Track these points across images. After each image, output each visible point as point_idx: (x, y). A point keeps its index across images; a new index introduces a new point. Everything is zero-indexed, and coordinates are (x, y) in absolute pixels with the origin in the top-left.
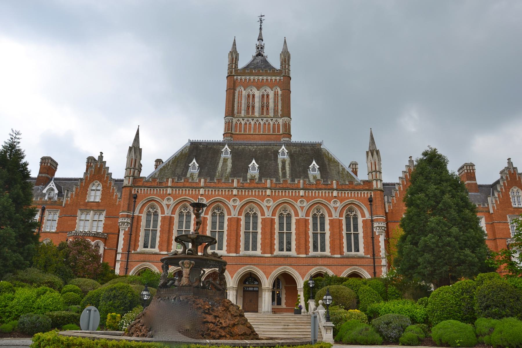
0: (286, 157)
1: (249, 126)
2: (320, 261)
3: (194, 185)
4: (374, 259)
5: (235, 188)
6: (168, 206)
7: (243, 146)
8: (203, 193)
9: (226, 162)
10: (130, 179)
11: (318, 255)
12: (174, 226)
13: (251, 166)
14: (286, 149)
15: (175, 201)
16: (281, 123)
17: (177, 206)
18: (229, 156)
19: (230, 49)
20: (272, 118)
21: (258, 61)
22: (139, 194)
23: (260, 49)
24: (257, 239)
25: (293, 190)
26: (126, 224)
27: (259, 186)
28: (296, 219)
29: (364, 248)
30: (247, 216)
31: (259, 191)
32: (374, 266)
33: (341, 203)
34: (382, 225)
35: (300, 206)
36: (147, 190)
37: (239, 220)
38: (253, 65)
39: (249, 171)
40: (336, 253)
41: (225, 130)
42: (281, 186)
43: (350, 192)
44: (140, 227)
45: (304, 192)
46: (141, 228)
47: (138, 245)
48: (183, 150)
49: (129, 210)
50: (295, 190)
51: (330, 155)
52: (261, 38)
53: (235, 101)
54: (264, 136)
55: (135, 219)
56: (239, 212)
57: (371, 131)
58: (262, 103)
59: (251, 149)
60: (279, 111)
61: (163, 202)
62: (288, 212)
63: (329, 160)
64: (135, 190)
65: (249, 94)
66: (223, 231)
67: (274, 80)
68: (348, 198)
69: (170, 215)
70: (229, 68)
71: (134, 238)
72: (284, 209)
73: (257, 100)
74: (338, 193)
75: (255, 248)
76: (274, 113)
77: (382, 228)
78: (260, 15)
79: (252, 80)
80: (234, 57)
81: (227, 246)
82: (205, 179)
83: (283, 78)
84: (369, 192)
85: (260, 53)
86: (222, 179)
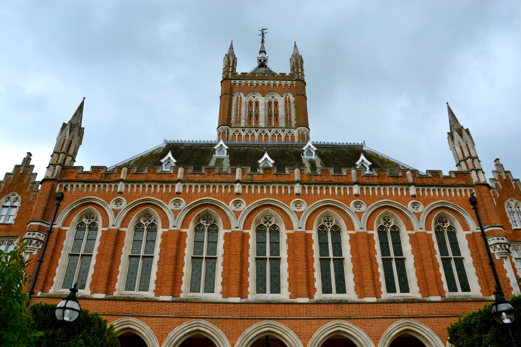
1: (251, 139)
2: (405, 310)
3: (166, 178)
5: (238, 181)
6: (116, 212)
7: (246, 148)
10: (55, 169)
11: (399, 298)
12: (124, 248)
15: (129, 204)
17: (132, 213)
20: (284, 128)
22: (66, 195)
24: (279, 271)
27: (281, 178)
28: (350, 234)
29: (480, 283)
30: (260, 230)
33: (425, 206)
36: (83, 186)
37: (244, 237)
40: (431, 293)
42: (319, 179)
45: (359, 188)
46: (62, 252)
47: (53, 282)
48: (154, 151)
49: (44, 218)
50: (344, 184)
52: (263, 50)
53: (232, 109)
55: (54, 235)
57: (448, 106)
60: (293, 120)
61: (108, 205)
62: (334, 223)
64: (61, 186)
65: (251, 101)
68: (435, 198)
71: (47, 268)
72: (326, 218)
75: (276, 288)
77: (505, 246)
78: (262, 29)
80: (231, 59)
81: (223, 284)
83: (296, 82)
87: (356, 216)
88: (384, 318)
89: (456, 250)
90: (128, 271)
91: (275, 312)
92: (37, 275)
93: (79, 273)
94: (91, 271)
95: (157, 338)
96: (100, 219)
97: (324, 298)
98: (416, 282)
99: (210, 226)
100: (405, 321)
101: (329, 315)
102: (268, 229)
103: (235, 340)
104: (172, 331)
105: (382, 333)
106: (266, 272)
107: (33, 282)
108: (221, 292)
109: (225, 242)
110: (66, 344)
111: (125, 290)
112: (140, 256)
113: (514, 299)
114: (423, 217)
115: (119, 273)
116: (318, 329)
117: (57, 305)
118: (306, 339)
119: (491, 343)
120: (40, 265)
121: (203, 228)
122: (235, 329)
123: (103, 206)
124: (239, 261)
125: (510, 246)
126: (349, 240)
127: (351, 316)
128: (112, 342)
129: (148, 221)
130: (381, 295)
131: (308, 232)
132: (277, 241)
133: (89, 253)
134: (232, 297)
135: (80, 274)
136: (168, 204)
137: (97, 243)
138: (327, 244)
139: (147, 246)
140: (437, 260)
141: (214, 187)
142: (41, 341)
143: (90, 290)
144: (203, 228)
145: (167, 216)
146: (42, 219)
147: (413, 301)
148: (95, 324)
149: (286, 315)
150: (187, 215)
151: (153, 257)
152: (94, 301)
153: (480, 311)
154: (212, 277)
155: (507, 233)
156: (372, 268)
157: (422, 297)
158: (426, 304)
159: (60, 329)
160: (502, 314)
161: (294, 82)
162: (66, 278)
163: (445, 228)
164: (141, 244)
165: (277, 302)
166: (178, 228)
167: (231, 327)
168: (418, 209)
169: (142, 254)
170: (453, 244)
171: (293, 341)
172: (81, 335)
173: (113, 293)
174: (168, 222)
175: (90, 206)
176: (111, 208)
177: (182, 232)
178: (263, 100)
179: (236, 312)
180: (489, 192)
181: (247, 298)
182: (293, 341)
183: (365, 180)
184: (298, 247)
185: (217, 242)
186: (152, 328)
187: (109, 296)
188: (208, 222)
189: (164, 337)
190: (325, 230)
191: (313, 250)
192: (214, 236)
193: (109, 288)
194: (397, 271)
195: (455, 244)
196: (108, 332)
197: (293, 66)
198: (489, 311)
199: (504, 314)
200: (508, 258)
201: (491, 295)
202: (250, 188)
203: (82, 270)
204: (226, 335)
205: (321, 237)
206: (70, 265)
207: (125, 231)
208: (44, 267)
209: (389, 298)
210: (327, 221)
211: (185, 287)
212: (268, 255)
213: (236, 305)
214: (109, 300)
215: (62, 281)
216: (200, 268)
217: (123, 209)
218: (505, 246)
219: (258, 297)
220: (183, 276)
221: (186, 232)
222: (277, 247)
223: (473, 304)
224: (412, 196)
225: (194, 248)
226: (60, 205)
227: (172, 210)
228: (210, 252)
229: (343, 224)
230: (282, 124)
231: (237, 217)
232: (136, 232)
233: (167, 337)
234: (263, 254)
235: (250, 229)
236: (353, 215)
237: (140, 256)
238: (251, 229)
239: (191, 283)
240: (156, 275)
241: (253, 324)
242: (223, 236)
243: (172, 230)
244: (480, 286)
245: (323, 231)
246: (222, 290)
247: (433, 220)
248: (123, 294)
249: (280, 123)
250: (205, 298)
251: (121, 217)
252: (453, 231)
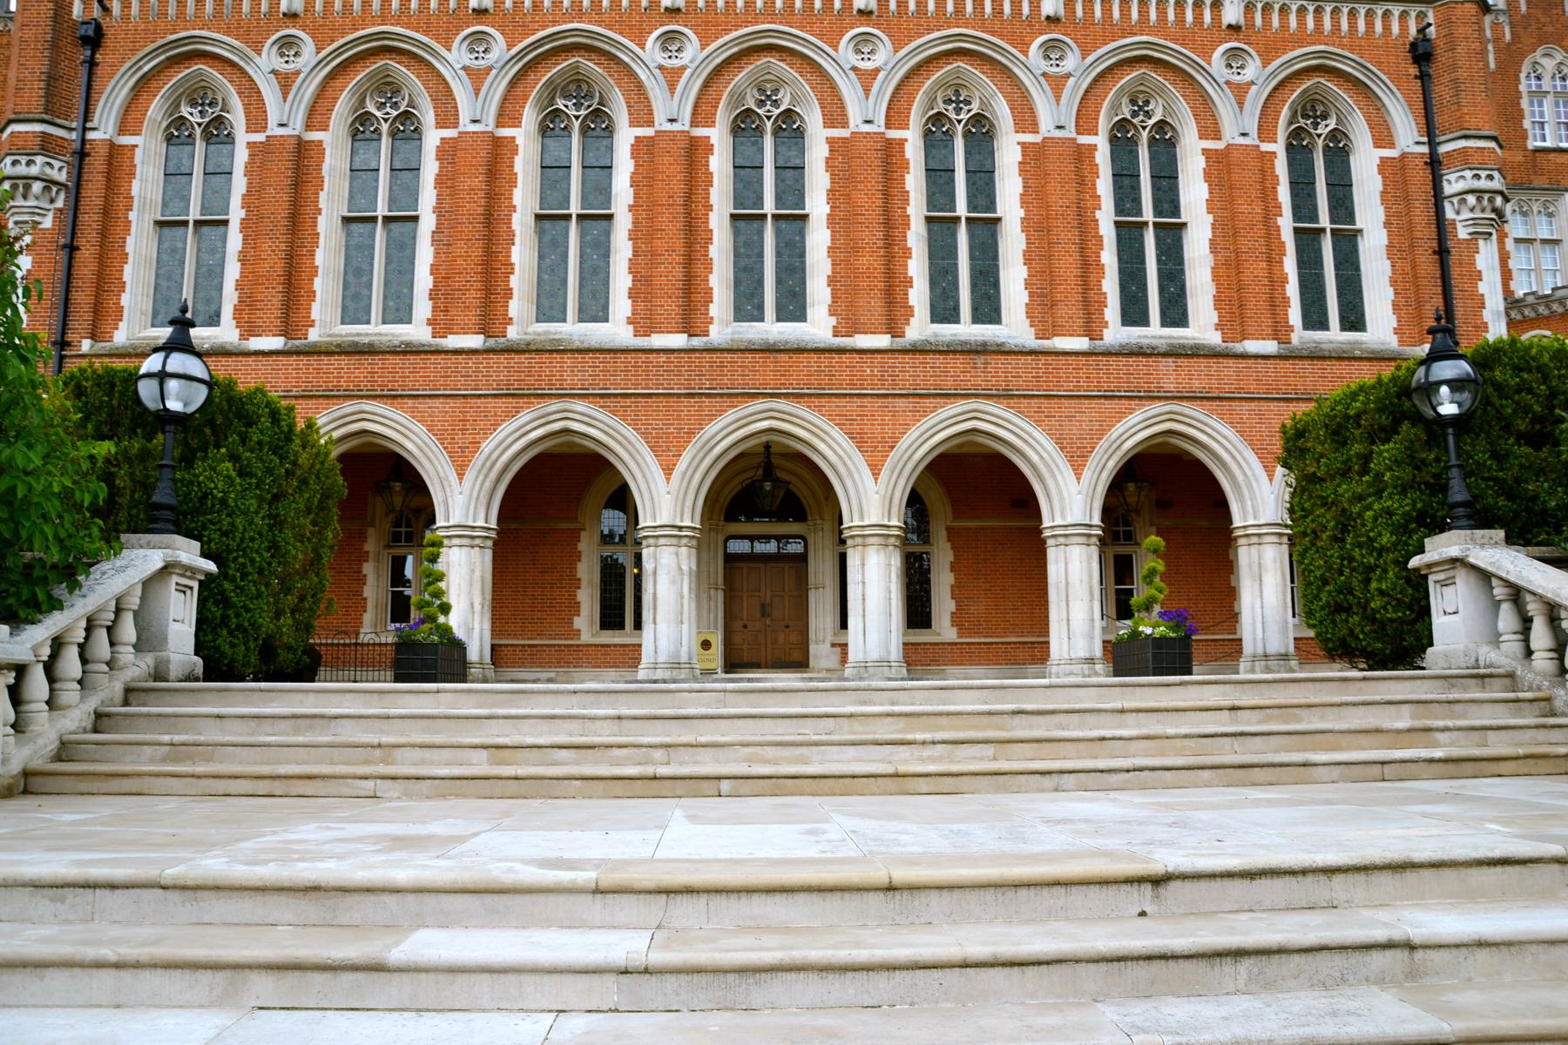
2: (1169, 375)
6: (285, 82)
11: (1155, 342)
12: (323, 196)
15: (324, 53)
17: (338, 83)
24: (802, 255)
26: (37, 187)
28: (1023, 145)
29: (1396, 307)
30: (744, 126)
33: (1265, 64)
37: (696, 151)
40: (1251, 330)
44: (129, 208)
46: (132, 216)
47: (120, 310)
49: (52, 109)
55: (96, 165)
61: (257, 59)
62: (975, 108)
68: (1300, 39)
69: (296, 127)
71: (93, 266)
72: (950, 93)
75: (793, 306)
77: (1491, 200)
81: (633, 294)
88: (1106, 397)
89: (1342, 205)
90: (346, 265)
91: (790, 375)
92: (68, 291)
93: (196, 278)
94: (232, 271)
95: (450, 457)
96: (237, 104)
98: (1211, 298)
99: (586, 116)
100: (1167, 408)
101: (949, 385)
102: (769, 124)
103: (673, 456)
104: (491, 434)
105: (1097, 439)
106: (763, 257)
107: (62, 314)
108: (628, 318)
109: (635, 166)
110: (187, 476)
111: (343, 323)
112: (376, 217)
113: (1483, 348)
114: (1255, 99)
115: (316, 271)
116: (914, 425)
117: (139, 369)
118: (879, 451)
119: (1395, 468)
120: (71, 258)
121: (566, 122)
122: (673, 424)
123: (242, 63)
124: (680, 225)
125: (1507, 200)
126: (1020, 163)
127: (1012, 390)
128: (318, 467)
129: (391, 107)
130: (1105, 330)
131: (894, 134)
132: (797, 162)
133: (219, 215)
134: (663, 332)
135: (200, 280)
136: (449, 50)
137: (239, 184)
138: (949, 173)
139: (396, 184)
140: (1279, 235)
142: (113, 469)
143: (237, 327)
144: (566, 122)
145: (449, 87)
146: (46, 114)
147: (1196, 352)
148: (259, 417)
149: (821, 384)
150: (513, 83)
151: (415, 219)
152: (253, 358)
153: (1380, 382)
154: (602, 276)
155: (1510, 159)
156: (1082, 250)
157: (1224, 342)
158: (1231, 362)
159: (160, 437)
160: (1438, 391)
162: (158, 296)
163: (1319, 136)
164: (377, 180)
165: (795, 346)
166: (488, 124)
167: (662, 420)
168: (1242, 72)
169: (382, 210)
170: (1337, 188)
171: (840, 457)
172: (223, 450)
173: (307, 334)
174: (456, 108)
175: (196, 64)
176: (267, 69)
177: (499, 138)
179: (675, 375)
180: (1479, 23)
181: (708, 335)
182: (840, 457)
184: (860, 182)
185: (611, 167)
186: (433, 430)
187: (297, 342)
188: (582, 104)
189: (470, 452)
190: (947, 131)
191: (908, 192)
192: (603, 149)
193: (292, 317)
194: (1159, 261)
195: (1341, 188)
196: (301, 439)
198: (1404, 380)
199: (1444, 390)
200: (1494, 237)
201: (1423, 343)
203: (204, 269)
204: (647, 442)
205: (934, 152)
206: (165, 257)
207: (321, 141)
208: (86, 266)
209: (1127, 341)
210: (953, 102)
212: (769, 207)
213: (676, 355)
214: (298, 353)
215: (148, 306)
216: (562, 249)
217: (306, 70)
218: (1491, 200)
219: (740, 333)
220: (512, 273)
221: (514, 138)
222: (797, 180)
224: (1230, 26)
225: (541, 188)
226: (97, 64)
227: (465, 68)
228: (591, 197)
229: (1003, 113)
231: (672, 87)
232: (356, 144)
233: (476, 452)
234: (755, 204)
235: (712, 124)
236: (1037, 84)
237: (376, 217)
238: (717, 125)
239: (538, 295)
240: (431, 274)
241: (726, 411)
242: (629, 147)
243: (468, 133)
244: (1395, 317)
245: (939, 134)
246: (633, 314)
247: (1286, 108)
248: (337, 336)
250: (582, 338)
251: (302, 97)
252: (1341, 145)
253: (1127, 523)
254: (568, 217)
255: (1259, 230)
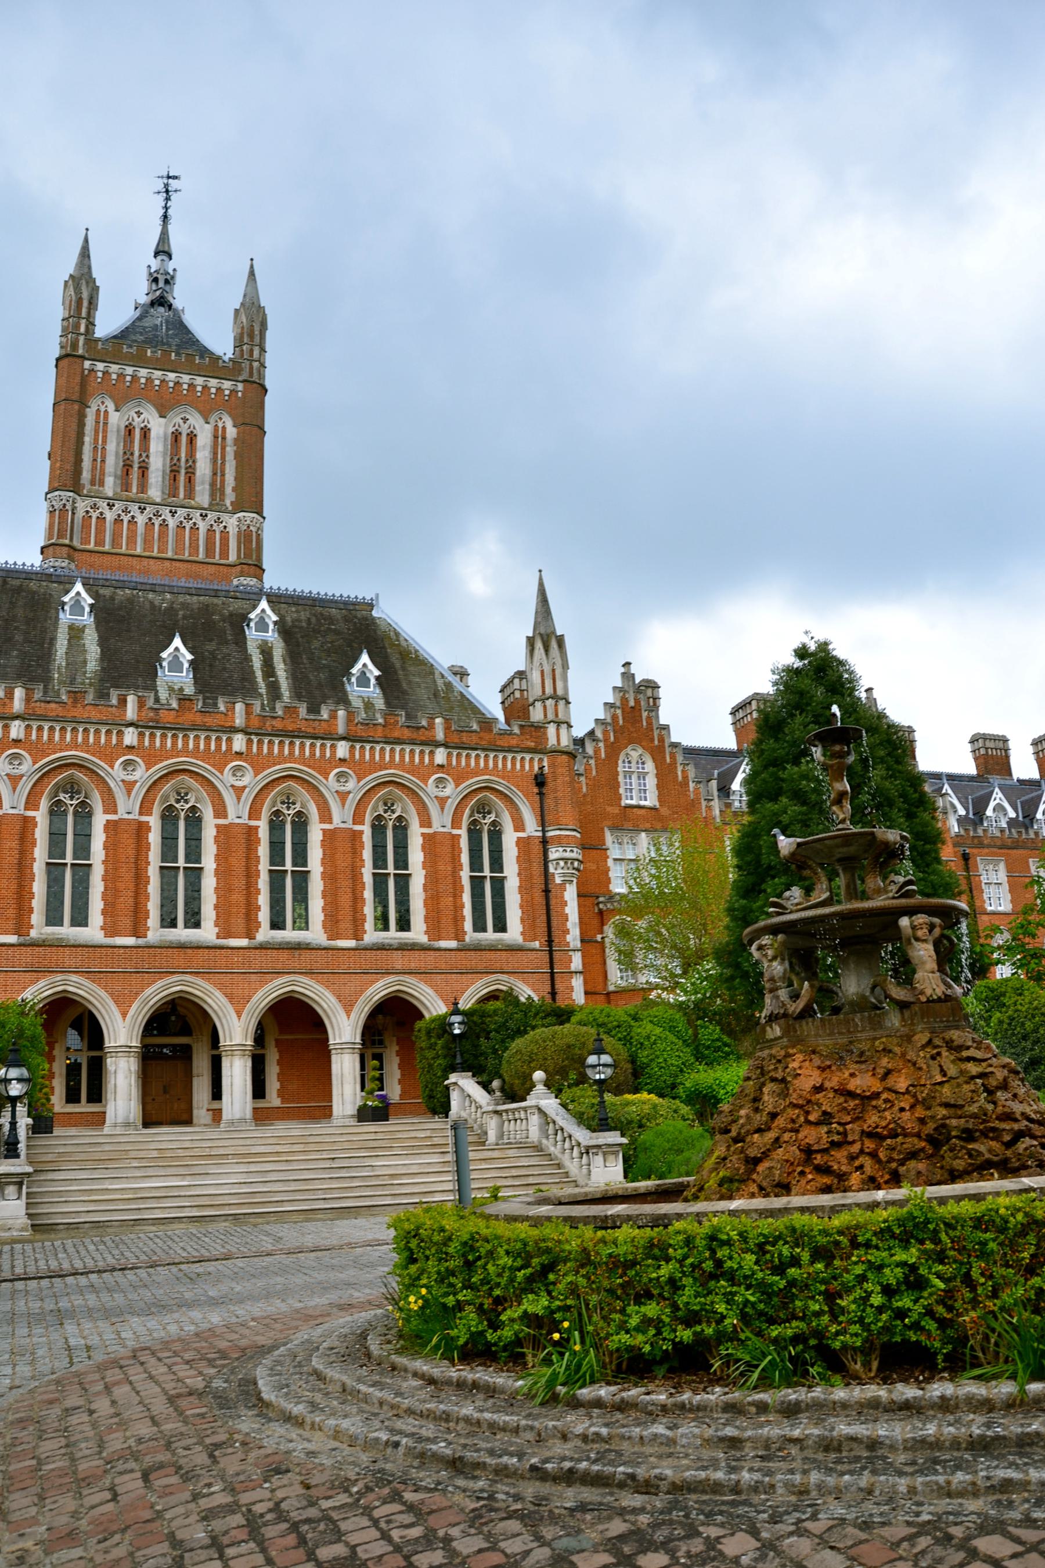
0: (271, 635)
1: (128, 529)
2: (398, 960)
4: (551, 952)
5: (131, 724)
7: (128, 591)
8: (22, 736)
9: (80, 638)
11: (392, 942)
13: (169, 655)
14: (273, 611)
16: (232, 531)
18: (87, 619)
19: (69, 266)
21: (158, 322)
23: (161, 284)
24: (199, 891)
25: (316, 738)
27: (209, 720)
28: (324, 830)
29: (522, 920)
30: (169, 817)
31: (208, 738)
32: (552, 974)
33: (457, 786)
34: (574, 855)
35: (337, 792)
37: (142, 829)
38: (141, 334)
39: (159, 674)
40: (443, 935)
41: (50, 535)
42: (278, 724)
43: (483, 755)
50: (323, 739)
51: (401, 639)
52: (166, 249)
53: (83, 443)
54: (178, 564)
56: (142, 803)
57: (541, 579)
58: (172, 459)
59: (156, 603)
62: (298, 807)
63: (401, 653)
65: (130, 424)
66: (90, 865)
67: (213, 390)
68: (477, 772)
70: (64, 329)
72: (284, 798)
73: (156, 447)
74: (449, 755)
76: (212, 495)
77: (572, 863)
78: (165, 174)
79: (143, 381)
80: (85, 295)
81: (104, 912)
82: (27, 689)
83: (244, 388)
84: (537, 757)
85: (162, 297)
86: (85, 692)
87: (338, 799)
97: (273, 938)
114: (451, 806)
124: (132, 875)
131: (253, 823)
141: (86, 731)
161: (239, 384)
178: (160, 426)
183: (360, 731)
197: (242, 335)
202: (152, 736)
211: (37, 918)
218: (572, 863)
223: (504, 954)
230: (203, 497)
231: (129, 792)
235: (151, 814)
249: (197, 494)
253: (380, 1035)
254: (66, 864)
255: (450, 880)
